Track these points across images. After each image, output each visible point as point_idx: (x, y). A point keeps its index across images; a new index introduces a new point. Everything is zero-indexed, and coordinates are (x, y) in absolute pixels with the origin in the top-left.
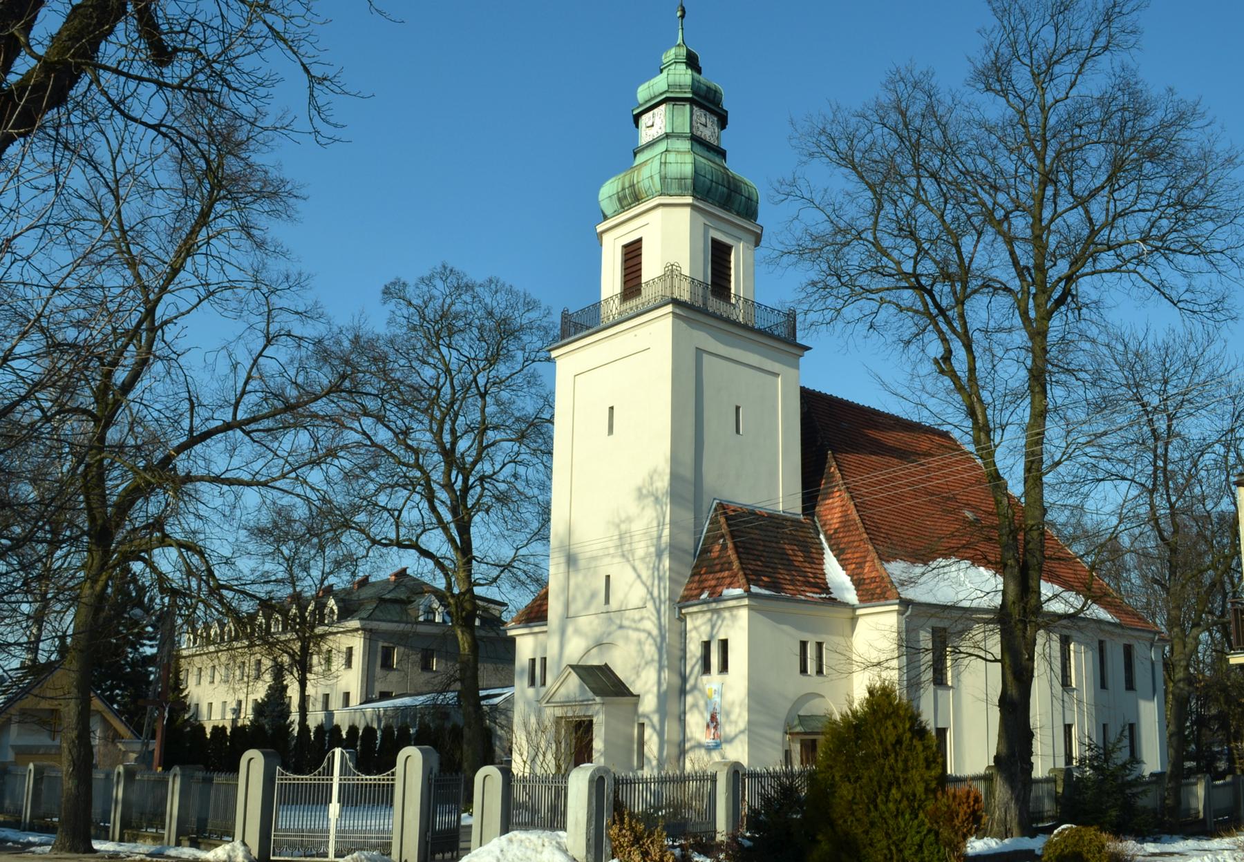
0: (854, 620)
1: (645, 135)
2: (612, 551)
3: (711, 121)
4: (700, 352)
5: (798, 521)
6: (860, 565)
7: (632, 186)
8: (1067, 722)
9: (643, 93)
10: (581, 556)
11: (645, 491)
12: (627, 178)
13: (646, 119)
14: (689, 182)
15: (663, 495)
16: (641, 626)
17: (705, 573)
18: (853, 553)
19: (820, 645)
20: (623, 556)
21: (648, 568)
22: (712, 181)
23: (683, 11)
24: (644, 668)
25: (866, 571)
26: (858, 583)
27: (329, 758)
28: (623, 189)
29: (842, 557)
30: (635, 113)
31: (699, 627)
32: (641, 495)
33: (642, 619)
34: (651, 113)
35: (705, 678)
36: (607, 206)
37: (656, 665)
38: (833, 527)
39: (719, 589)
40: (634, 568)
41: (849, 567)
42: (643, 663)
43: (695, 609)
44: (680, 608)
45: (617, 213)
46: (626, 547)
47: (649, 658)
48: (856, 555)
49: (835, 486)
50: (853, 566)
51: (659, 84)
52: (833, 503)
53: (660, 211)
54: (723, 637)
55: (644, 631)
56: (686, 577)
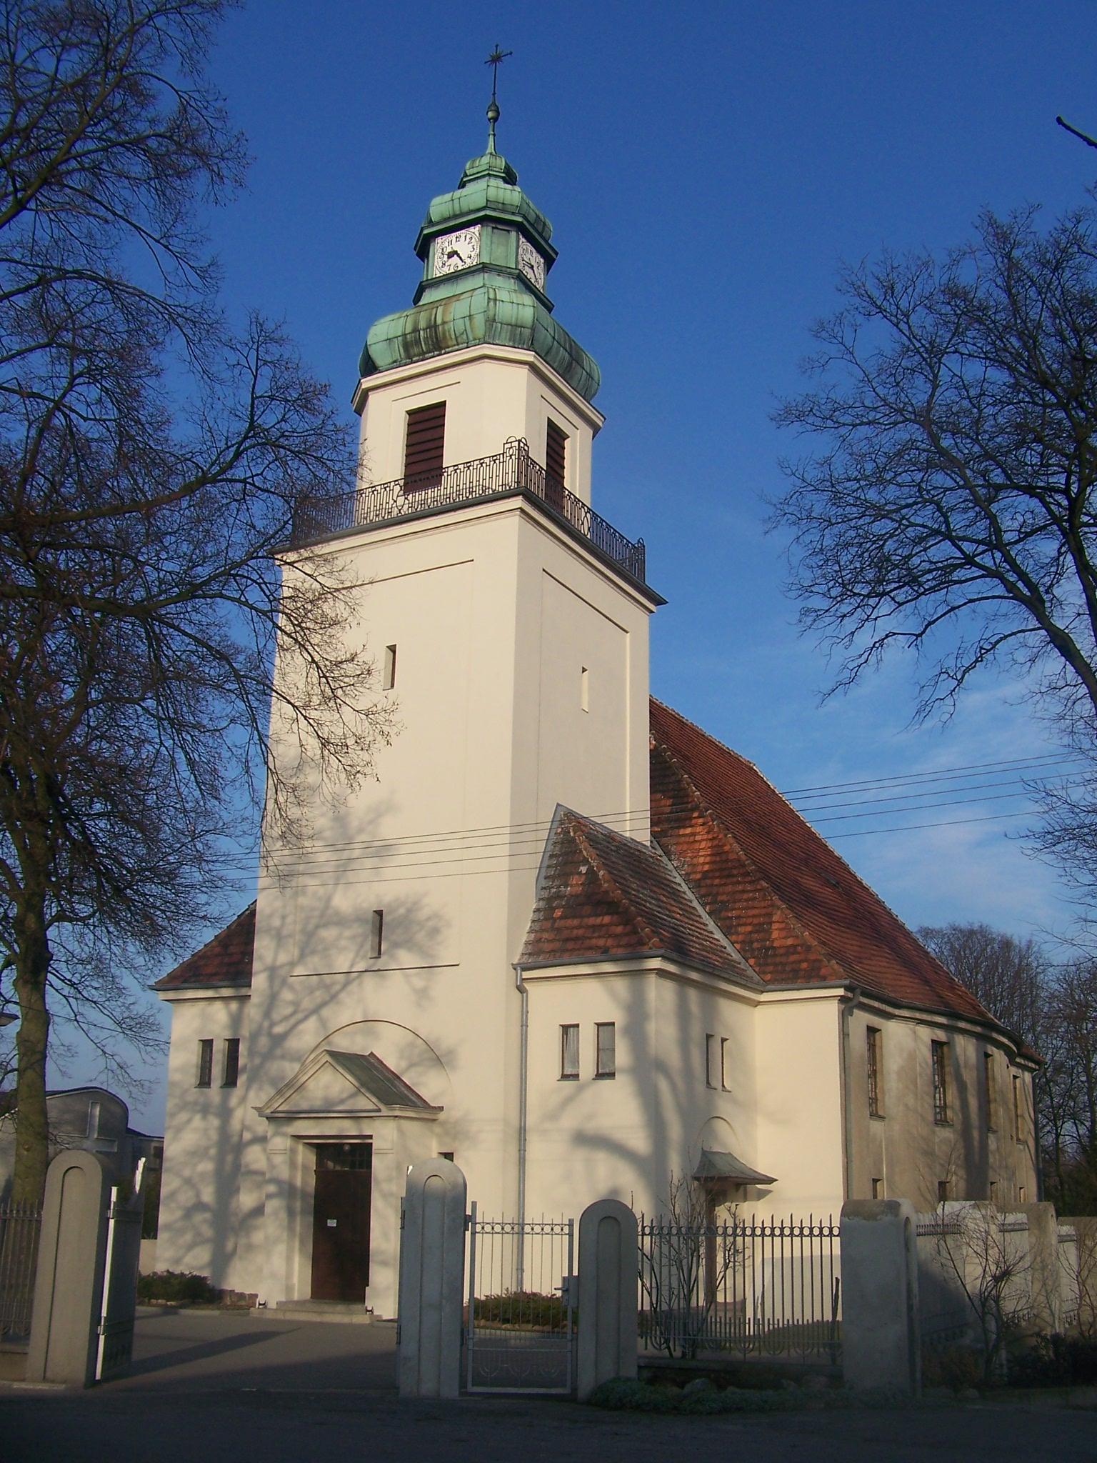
1: (439, 265)
3: (536, 259)
7: (432, 326)
9: (440, 206)
13: (441, 245)
14: (527, 332)
23: (497, 112)
25: (775, 935)
28: (416, 330)
30: (426, 232)
36: (380, 354)
38: (699, 868)
45: (396, 364)
49: (693, 810)
50: (749, 928)
51: (474, 195)
52: (694, 834)
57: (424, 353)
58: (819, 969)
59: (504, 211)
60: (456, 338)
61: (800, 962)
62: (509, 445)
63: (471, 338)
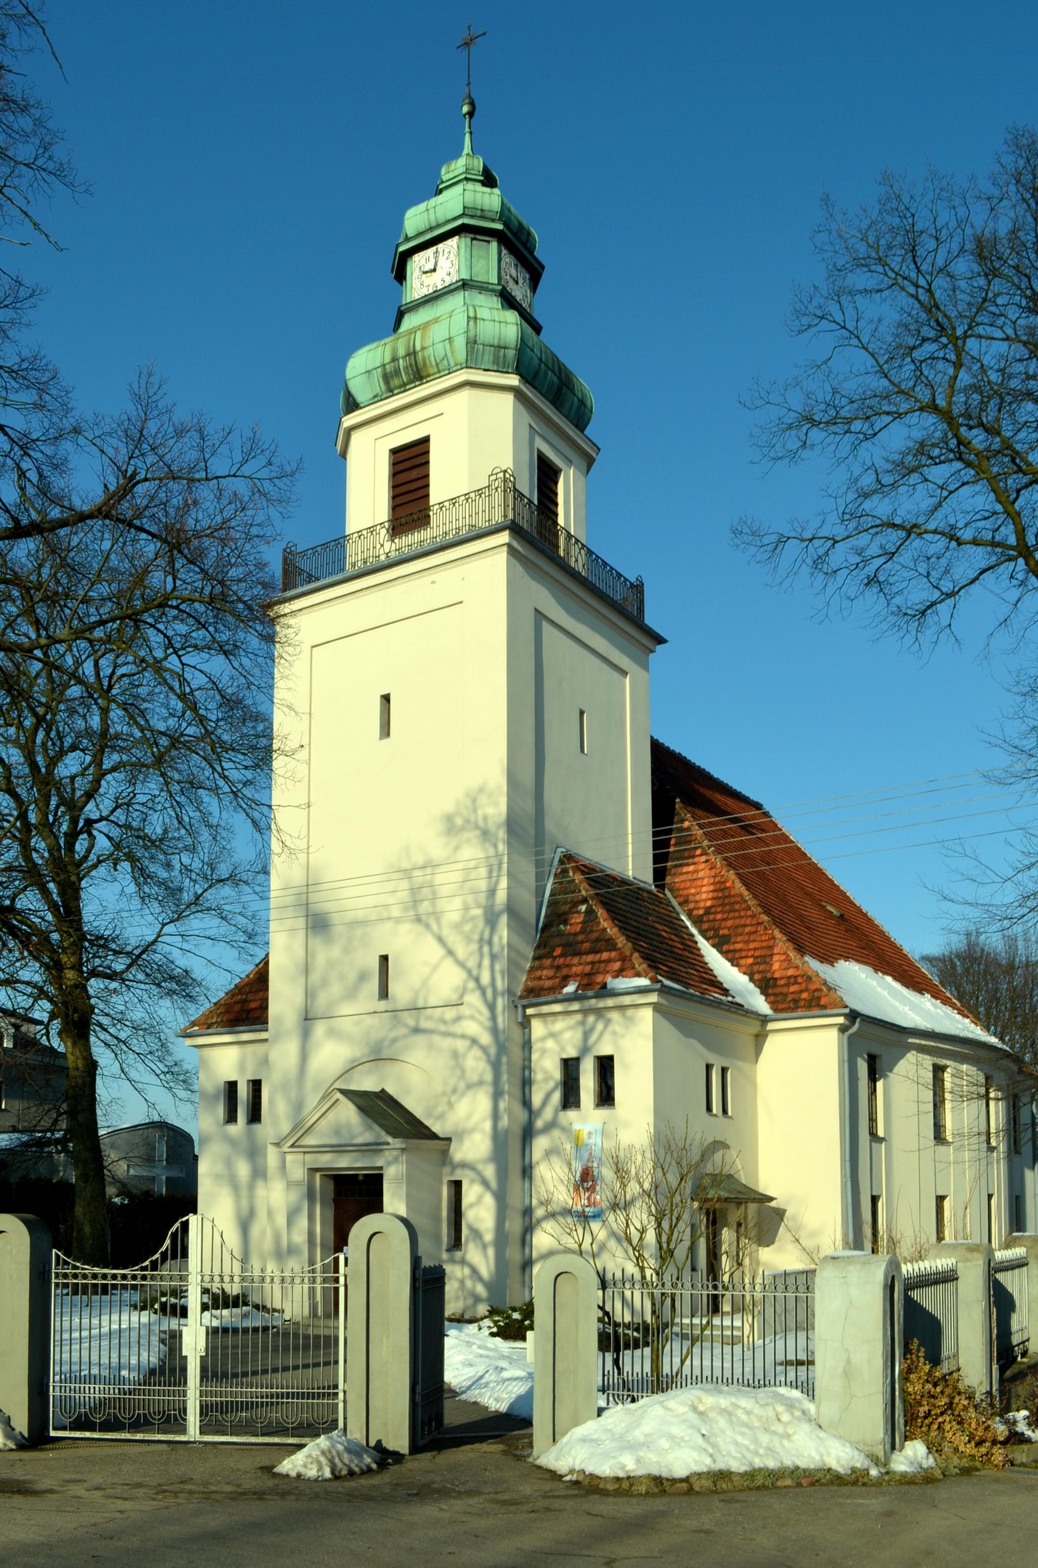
0: (760, 1039)
2: (396, 912)
3: (523, 276)
4: (540, 615)
5: (649, 892)
6: (765, 959)
7: (412, 354)
8: (940, 1193)
10: (336, 919)
11: (459, 821)
12: (388, 348)
13: (419, 262)
14: (511, 353)
15: (499, 827)
16: (458, 1029)
17: (561, 956)
18: (747, 942)
19: (724, 1071)
20: (418, 920)
21: (468, 940)
22: (540, 360)
24: (463, 1094)
26: (766, 985)
27: (174, 1236)
28: (395, 359)
29: (725, 948)
30: (401, 249)
31: (560, 1033)
32: (451, 826)
33: (458, 1019)
34: (432, 250)
35: (571, 1114)
36: (360, 389)
37: (490, 1089)
38: (702, 904)
39: (599, 979)
40: (441, 940)
41: (743, 962)
42: (462, 1085)
43: (557, 1008)
44: (525, 1007)
45: (377, 399)
46: (425, 907)
47: (475, 1078)
48: (752, 946)
49: (696, 848)
50: (750, 961)
52: (696, 871)
53: (466, 393)
54: (605, 1050)
55: (463, 1036)
56: (526, 959)
57: (404, 385)
58: (819, 998)
59: (483, 217)
60: (437, 365)
61: (801, 991)
62: (494, 477)
63: (452, 364)
